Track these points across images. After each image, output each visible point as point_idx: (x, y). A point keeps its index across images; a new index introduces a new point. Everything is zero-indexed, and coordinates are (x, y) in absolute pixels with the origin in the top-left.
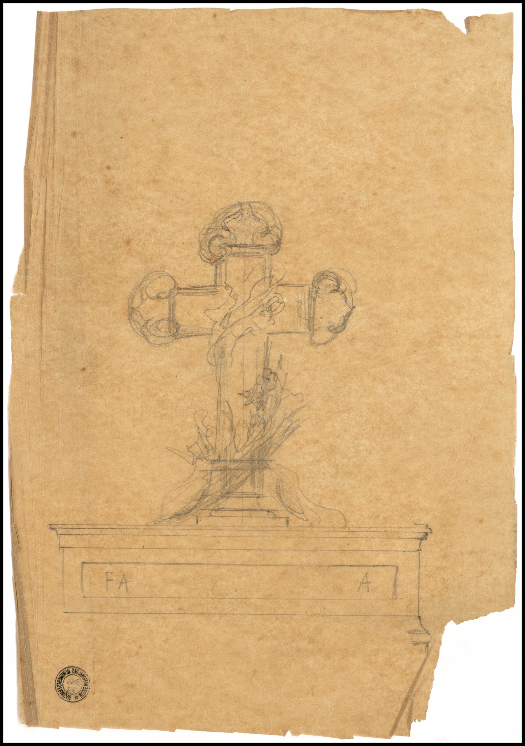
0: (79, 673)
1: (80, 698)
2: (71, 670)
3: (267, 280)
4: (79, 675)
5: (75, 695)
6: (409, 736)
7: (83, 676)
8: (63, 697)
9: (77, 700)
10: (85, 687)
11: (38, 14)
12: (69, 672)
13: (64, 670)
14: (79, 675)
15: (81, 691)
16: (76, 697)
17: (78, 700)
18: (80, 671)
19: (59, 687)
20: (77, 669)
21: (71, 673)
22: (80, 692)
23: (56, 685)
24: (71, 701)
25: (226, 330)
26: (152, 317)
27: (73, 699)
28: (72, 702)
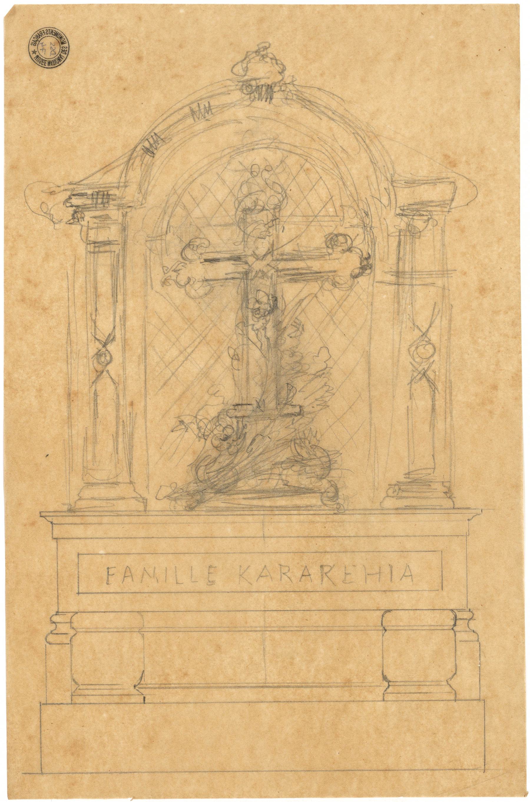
0: (62, 54)
1: (34, 56)
2: (66, 45)
3: (289, 102)
4: (60, 55)
5: (36, 50)
6: (517, 7)
7: (59, 59)
8: (34, 36)
9: (31, 53)
10: (47, 62)
11: (15, 798)
12: (62, 43)
13: (64, 37)
14: (60, 55)
15: (42, 58)
16: (34, 52)
17: (31, 55)
18: (65, 56)
19: (45, 32)
20: (67, 52)
21: (62, 46)
22: (40, 56)
23: (48, 29)
24: (30, 45)
25: (153, 130)
26: (411, 366)
27: (32, 48)
28: (185, 106)
